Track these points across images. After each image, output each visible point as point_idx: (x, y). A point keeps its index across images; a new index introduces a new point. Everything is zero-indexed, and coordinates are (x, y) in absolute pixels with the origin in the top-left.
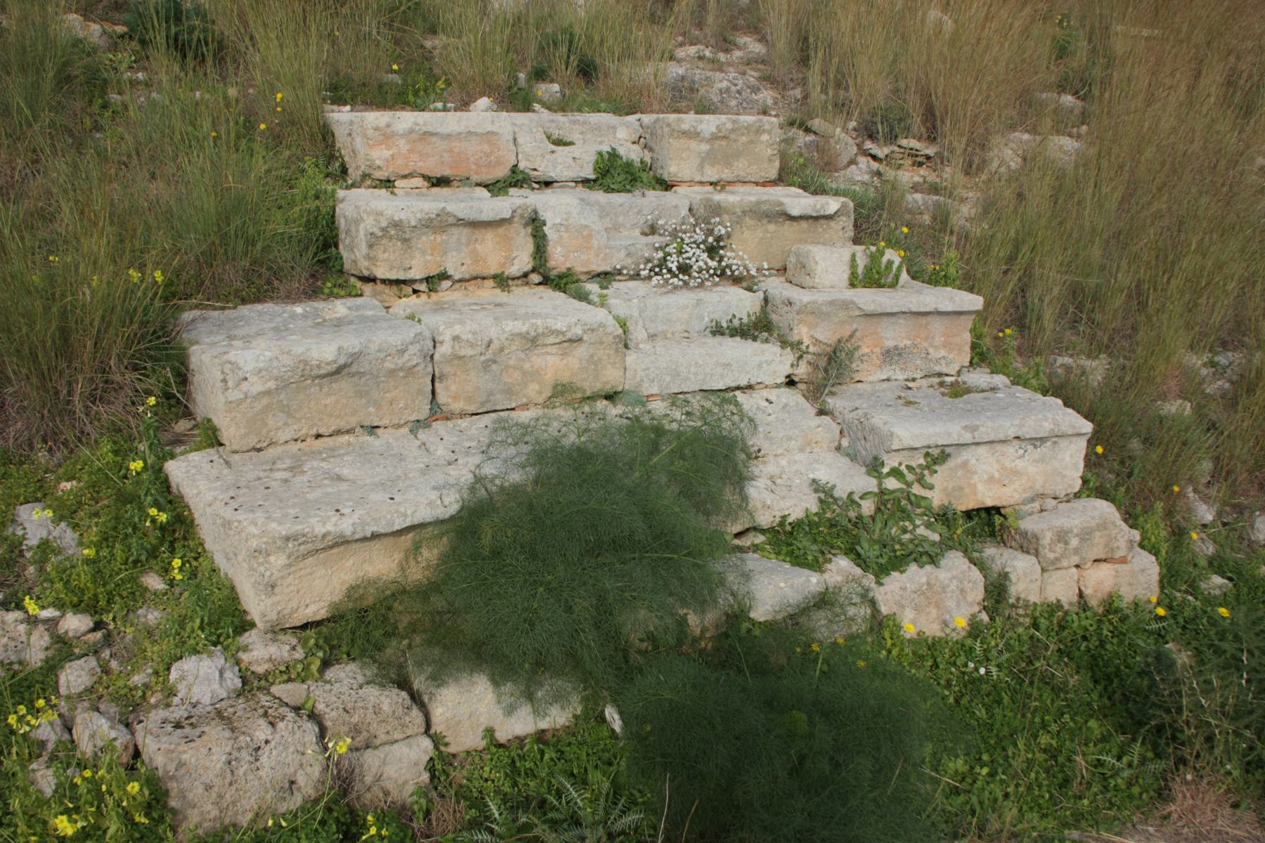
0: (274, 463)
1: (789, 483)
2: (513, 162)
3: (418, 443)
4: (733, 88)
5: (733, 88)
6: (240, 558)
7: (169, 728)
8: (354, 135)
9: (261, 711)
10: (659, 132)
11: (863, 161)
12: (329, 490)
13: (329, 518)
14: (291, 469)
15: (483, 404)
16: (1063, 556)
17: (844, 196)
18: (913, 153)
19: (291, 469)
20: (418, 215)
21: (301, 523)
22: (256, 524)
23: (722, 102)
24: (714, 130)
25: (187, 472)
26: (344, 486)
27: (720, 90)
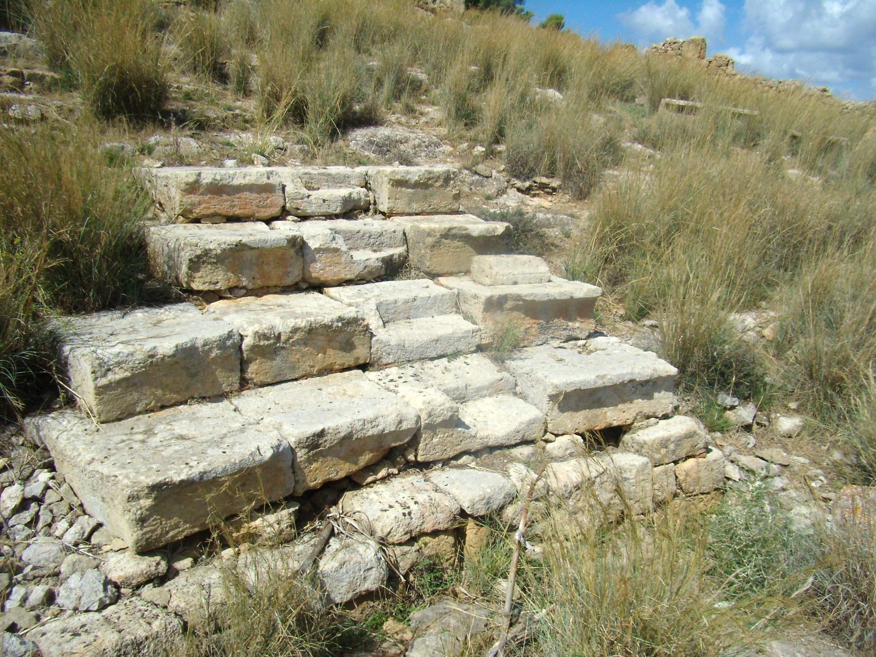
0: (132, 428)
1: (485, 419)
2: (282, 203)
3: (233, 407)
4: (423, 144)
5: (423, 144)
6: (116, 502)
7: (68, 636)
8: (170, 186)
9: (139, 614)
10: (380, 180)
11: (512, 192)
12: (177, 448)
13: (182, 470)
14: (145, 432)
15: (275, 377)
16: (665, 456)
17: (509, 222)
18: (543, 186)
19: (145, 432)
20: (223, 246)
21: (162, 475)
22: (128, 478)
23: (415, 154)
24: (417, 178)
25: (68, 439)
26: (188, 443)
27: (414, 145)
